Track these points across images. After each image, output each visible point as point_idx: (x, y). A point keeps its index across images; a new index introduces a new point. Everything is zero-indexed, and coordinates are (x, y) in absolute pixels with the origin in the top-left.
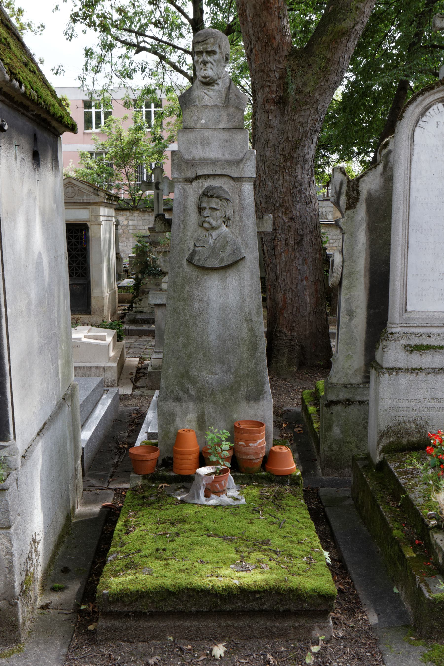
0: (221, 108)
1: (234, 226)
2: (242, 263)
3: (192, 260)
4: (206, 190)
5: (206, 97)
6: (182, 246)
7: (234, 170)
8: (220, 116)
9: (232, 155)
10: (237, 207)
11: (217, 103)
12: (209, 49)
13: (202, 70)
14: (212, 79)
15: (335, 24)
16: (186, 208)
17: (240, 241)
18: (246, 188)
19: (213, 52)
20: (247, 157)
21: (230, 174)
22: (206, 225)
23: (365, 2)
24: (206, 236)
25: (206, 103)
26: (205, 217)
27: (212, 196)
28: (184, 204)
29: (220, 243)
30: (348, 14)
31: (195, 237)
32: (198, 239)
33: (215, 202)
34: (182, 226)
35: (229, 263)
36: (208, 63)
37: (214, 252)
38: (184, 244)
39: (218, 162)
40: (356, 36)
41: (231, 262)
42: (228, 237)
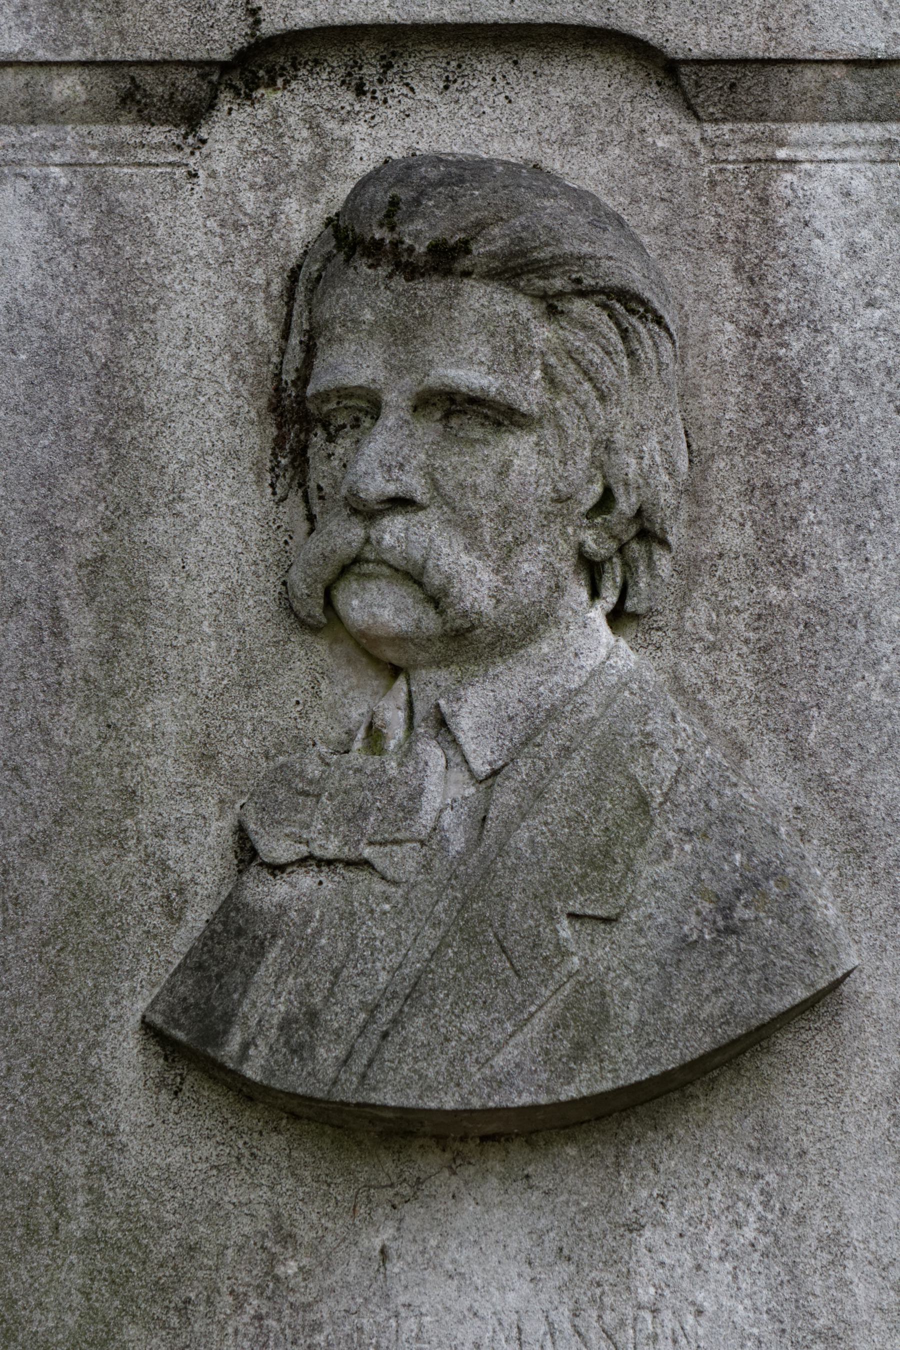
1: (700, 614)
2: (811, 1048)
3: (215, 1035)
4: (381, 196)
6: (91, 862)
10: (727, 403)
16: (135, 411)
17: (770, 786)
18: (821, 188)
21: (637, 24)
22: (379, 607)
24: (375, 736)
26: (368, 513)
27: (445, 259)
28: (109, 368)
29: (556, 809)
31: (239, 750)
32: (283, 776)
33: (485, 324)
34: (83, 628)
35: (669, 1059)
37: (482, 924)
38: (113, 838)
41: (700, 1044)
42: (649, 743)
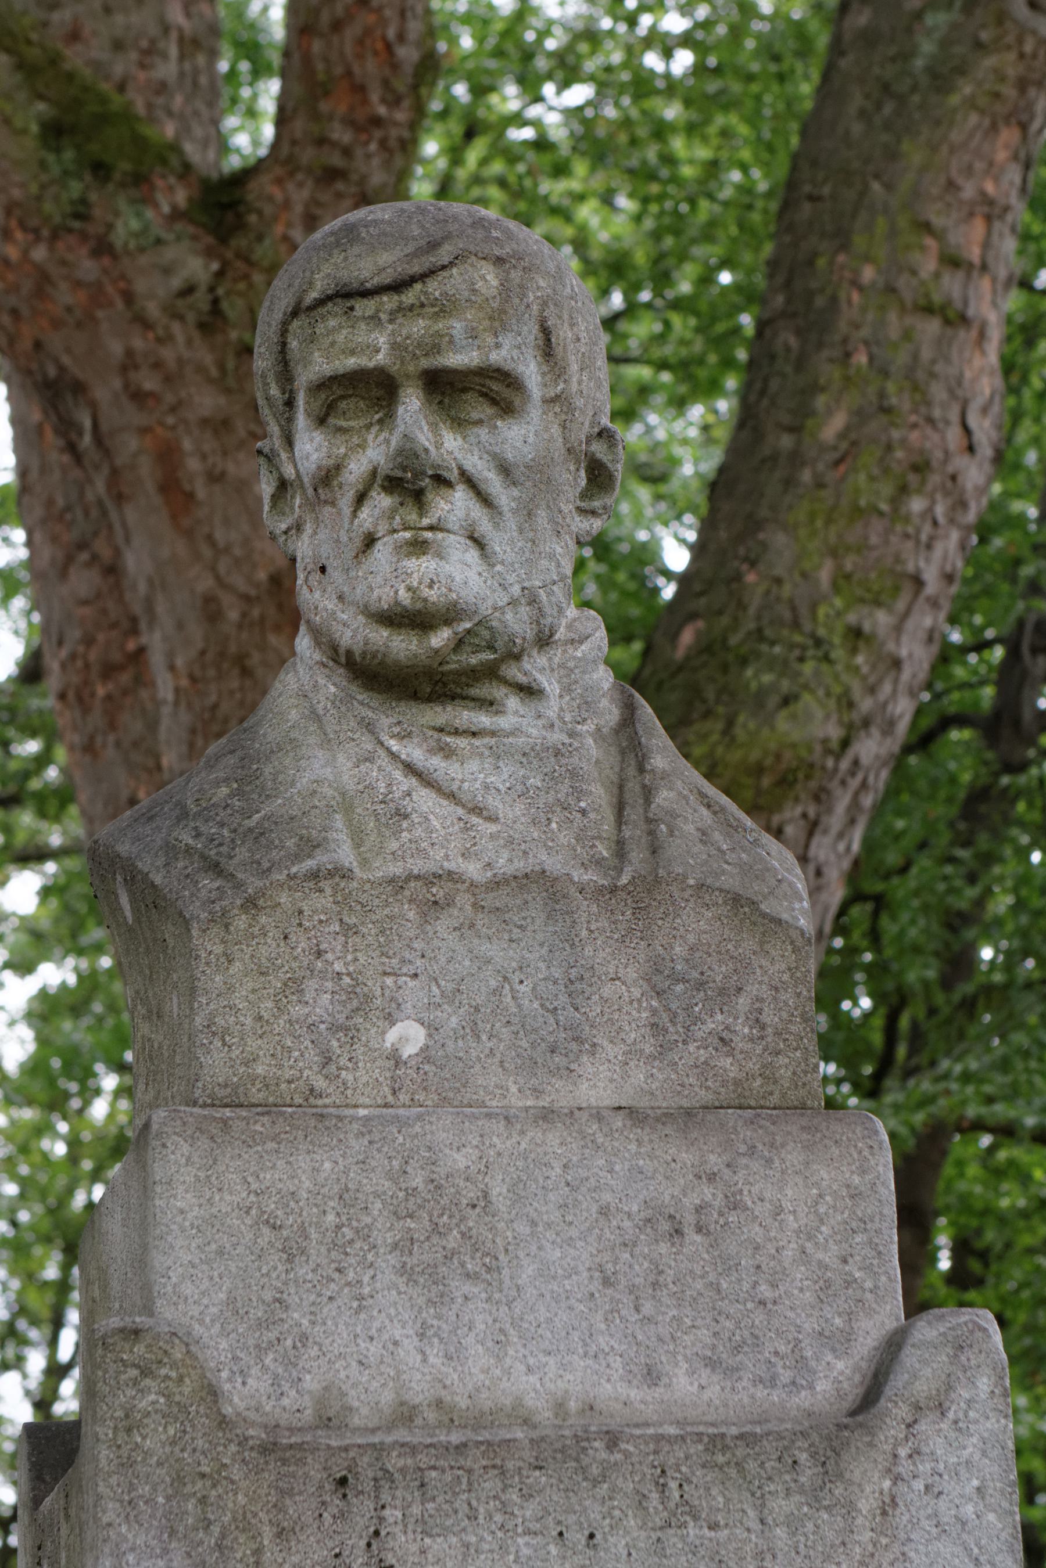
0: (585, 909)
5: (425, 800)
7: (793, 1524)
8: (576, 984)
9: (732, 1372)
11: (554, 864)
12: (457, 359)
13: (382, 552)
14: (480, 634)
15: (730, 723)
19: (490, 391)
20: (923, 1389)
23: (901, 605)
25: (437, 859)
30: (808, 668)
36: (441, 481)
39: (612, 1440)
40: (855, 804)
